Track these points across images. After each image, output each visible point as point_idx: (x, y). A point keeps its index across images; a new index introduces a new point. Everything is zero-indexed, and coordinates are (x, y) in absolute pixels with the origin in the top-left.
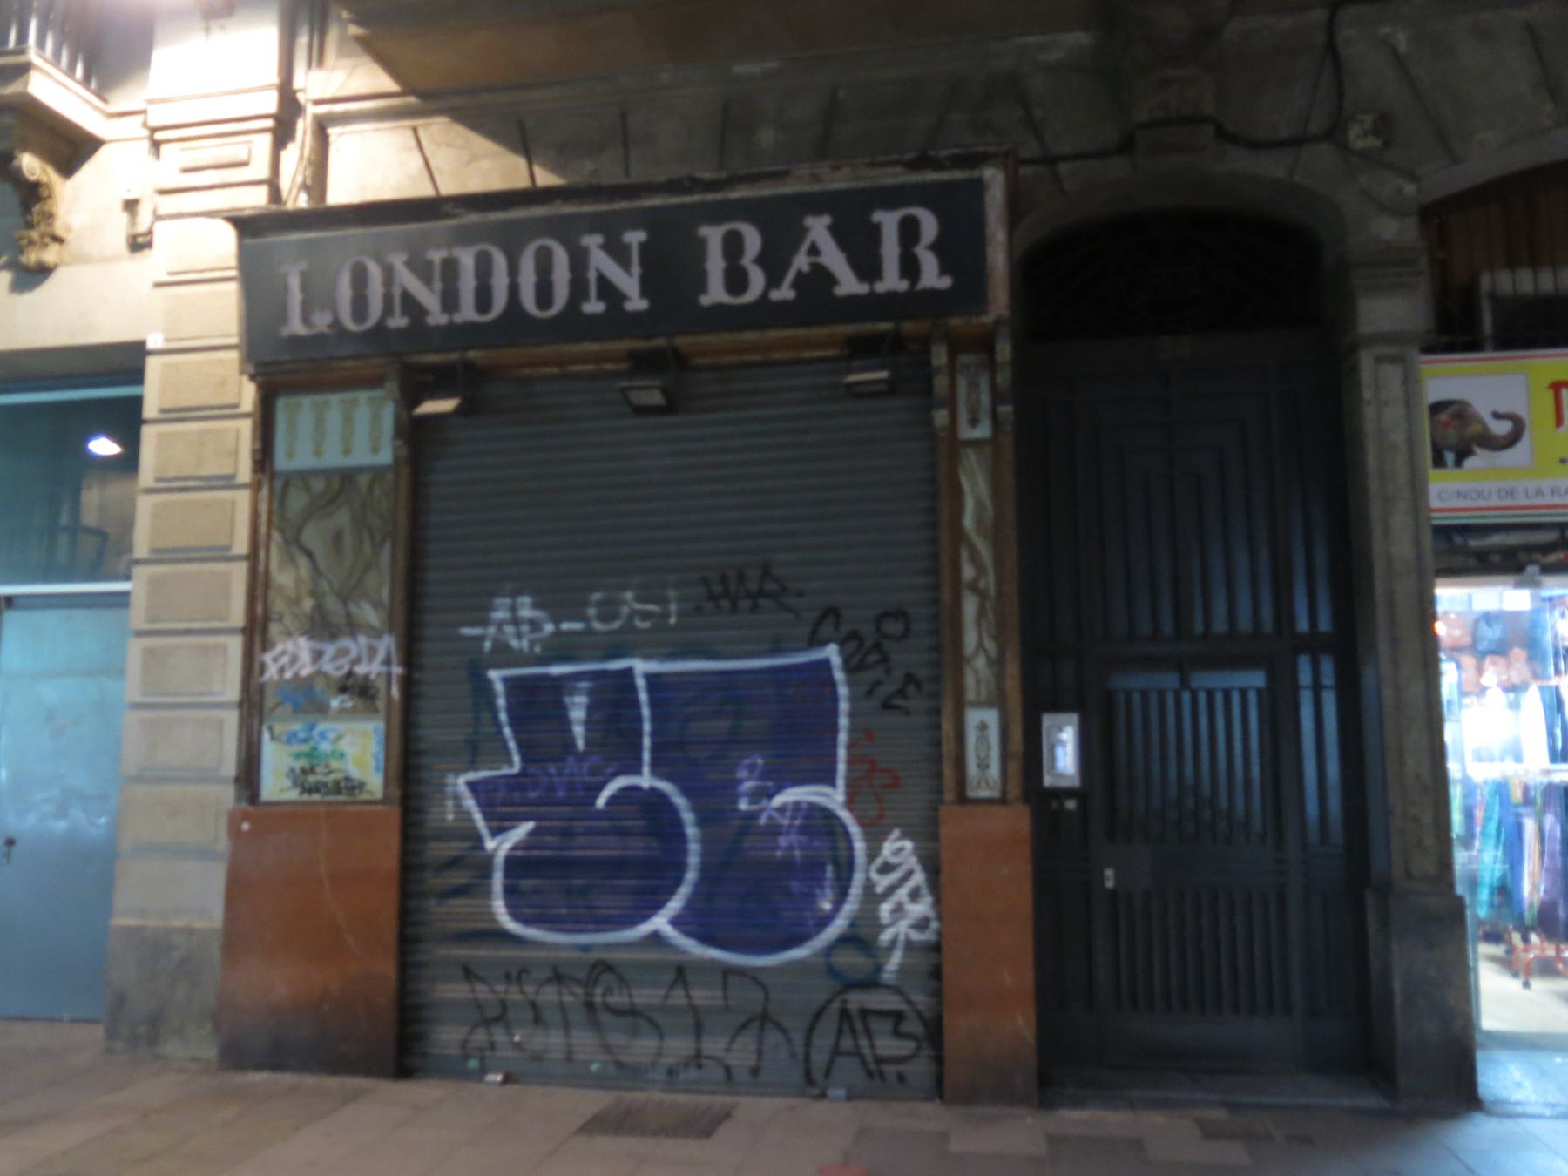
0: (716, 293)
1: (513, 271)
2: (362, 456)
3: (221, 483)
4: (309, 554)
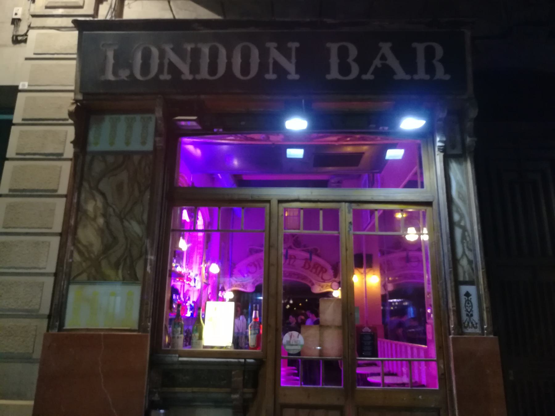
0: (334, 74)
1: (229, 57)
2: (135, 146)
3: (55, 157)
4: (103, 194)
